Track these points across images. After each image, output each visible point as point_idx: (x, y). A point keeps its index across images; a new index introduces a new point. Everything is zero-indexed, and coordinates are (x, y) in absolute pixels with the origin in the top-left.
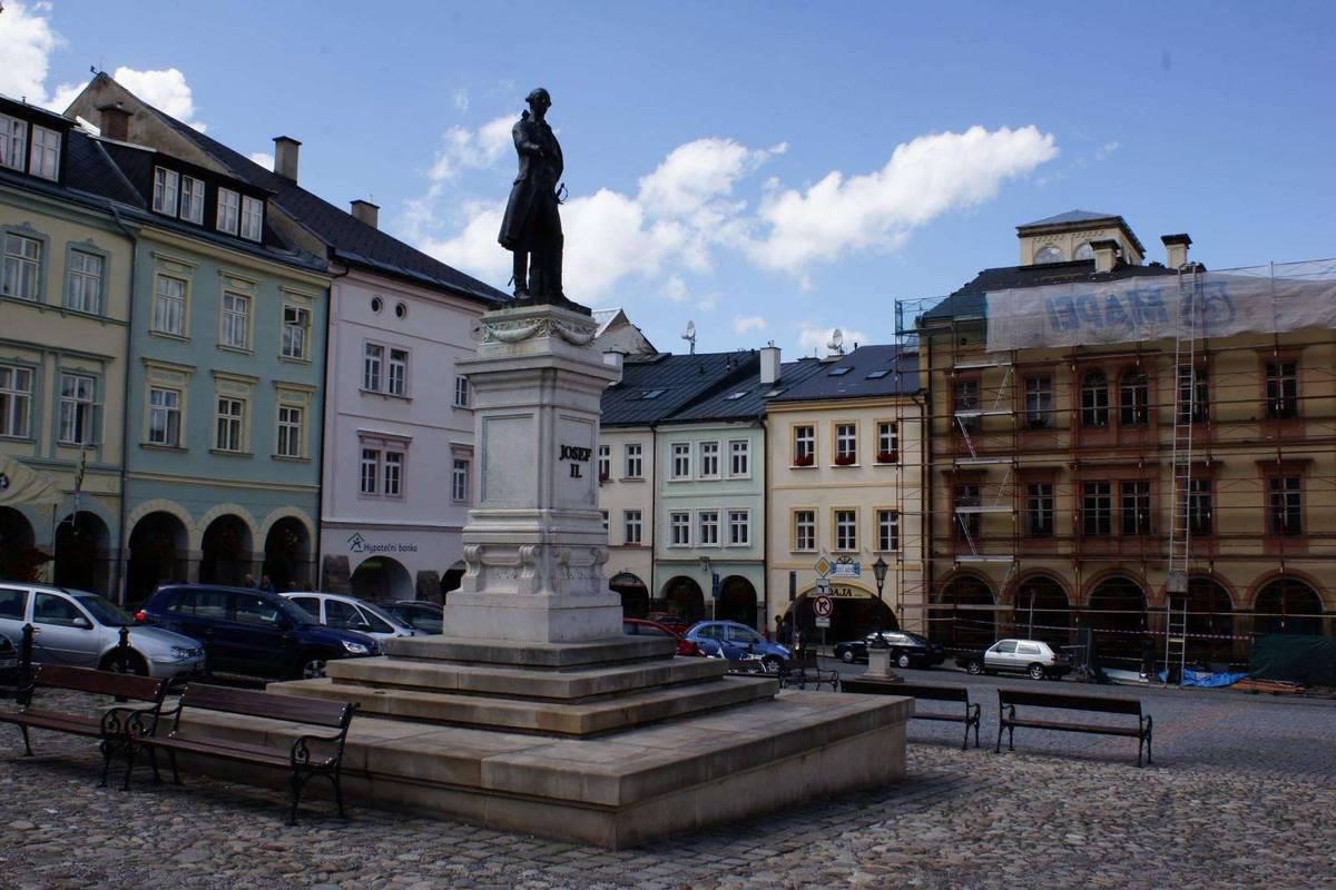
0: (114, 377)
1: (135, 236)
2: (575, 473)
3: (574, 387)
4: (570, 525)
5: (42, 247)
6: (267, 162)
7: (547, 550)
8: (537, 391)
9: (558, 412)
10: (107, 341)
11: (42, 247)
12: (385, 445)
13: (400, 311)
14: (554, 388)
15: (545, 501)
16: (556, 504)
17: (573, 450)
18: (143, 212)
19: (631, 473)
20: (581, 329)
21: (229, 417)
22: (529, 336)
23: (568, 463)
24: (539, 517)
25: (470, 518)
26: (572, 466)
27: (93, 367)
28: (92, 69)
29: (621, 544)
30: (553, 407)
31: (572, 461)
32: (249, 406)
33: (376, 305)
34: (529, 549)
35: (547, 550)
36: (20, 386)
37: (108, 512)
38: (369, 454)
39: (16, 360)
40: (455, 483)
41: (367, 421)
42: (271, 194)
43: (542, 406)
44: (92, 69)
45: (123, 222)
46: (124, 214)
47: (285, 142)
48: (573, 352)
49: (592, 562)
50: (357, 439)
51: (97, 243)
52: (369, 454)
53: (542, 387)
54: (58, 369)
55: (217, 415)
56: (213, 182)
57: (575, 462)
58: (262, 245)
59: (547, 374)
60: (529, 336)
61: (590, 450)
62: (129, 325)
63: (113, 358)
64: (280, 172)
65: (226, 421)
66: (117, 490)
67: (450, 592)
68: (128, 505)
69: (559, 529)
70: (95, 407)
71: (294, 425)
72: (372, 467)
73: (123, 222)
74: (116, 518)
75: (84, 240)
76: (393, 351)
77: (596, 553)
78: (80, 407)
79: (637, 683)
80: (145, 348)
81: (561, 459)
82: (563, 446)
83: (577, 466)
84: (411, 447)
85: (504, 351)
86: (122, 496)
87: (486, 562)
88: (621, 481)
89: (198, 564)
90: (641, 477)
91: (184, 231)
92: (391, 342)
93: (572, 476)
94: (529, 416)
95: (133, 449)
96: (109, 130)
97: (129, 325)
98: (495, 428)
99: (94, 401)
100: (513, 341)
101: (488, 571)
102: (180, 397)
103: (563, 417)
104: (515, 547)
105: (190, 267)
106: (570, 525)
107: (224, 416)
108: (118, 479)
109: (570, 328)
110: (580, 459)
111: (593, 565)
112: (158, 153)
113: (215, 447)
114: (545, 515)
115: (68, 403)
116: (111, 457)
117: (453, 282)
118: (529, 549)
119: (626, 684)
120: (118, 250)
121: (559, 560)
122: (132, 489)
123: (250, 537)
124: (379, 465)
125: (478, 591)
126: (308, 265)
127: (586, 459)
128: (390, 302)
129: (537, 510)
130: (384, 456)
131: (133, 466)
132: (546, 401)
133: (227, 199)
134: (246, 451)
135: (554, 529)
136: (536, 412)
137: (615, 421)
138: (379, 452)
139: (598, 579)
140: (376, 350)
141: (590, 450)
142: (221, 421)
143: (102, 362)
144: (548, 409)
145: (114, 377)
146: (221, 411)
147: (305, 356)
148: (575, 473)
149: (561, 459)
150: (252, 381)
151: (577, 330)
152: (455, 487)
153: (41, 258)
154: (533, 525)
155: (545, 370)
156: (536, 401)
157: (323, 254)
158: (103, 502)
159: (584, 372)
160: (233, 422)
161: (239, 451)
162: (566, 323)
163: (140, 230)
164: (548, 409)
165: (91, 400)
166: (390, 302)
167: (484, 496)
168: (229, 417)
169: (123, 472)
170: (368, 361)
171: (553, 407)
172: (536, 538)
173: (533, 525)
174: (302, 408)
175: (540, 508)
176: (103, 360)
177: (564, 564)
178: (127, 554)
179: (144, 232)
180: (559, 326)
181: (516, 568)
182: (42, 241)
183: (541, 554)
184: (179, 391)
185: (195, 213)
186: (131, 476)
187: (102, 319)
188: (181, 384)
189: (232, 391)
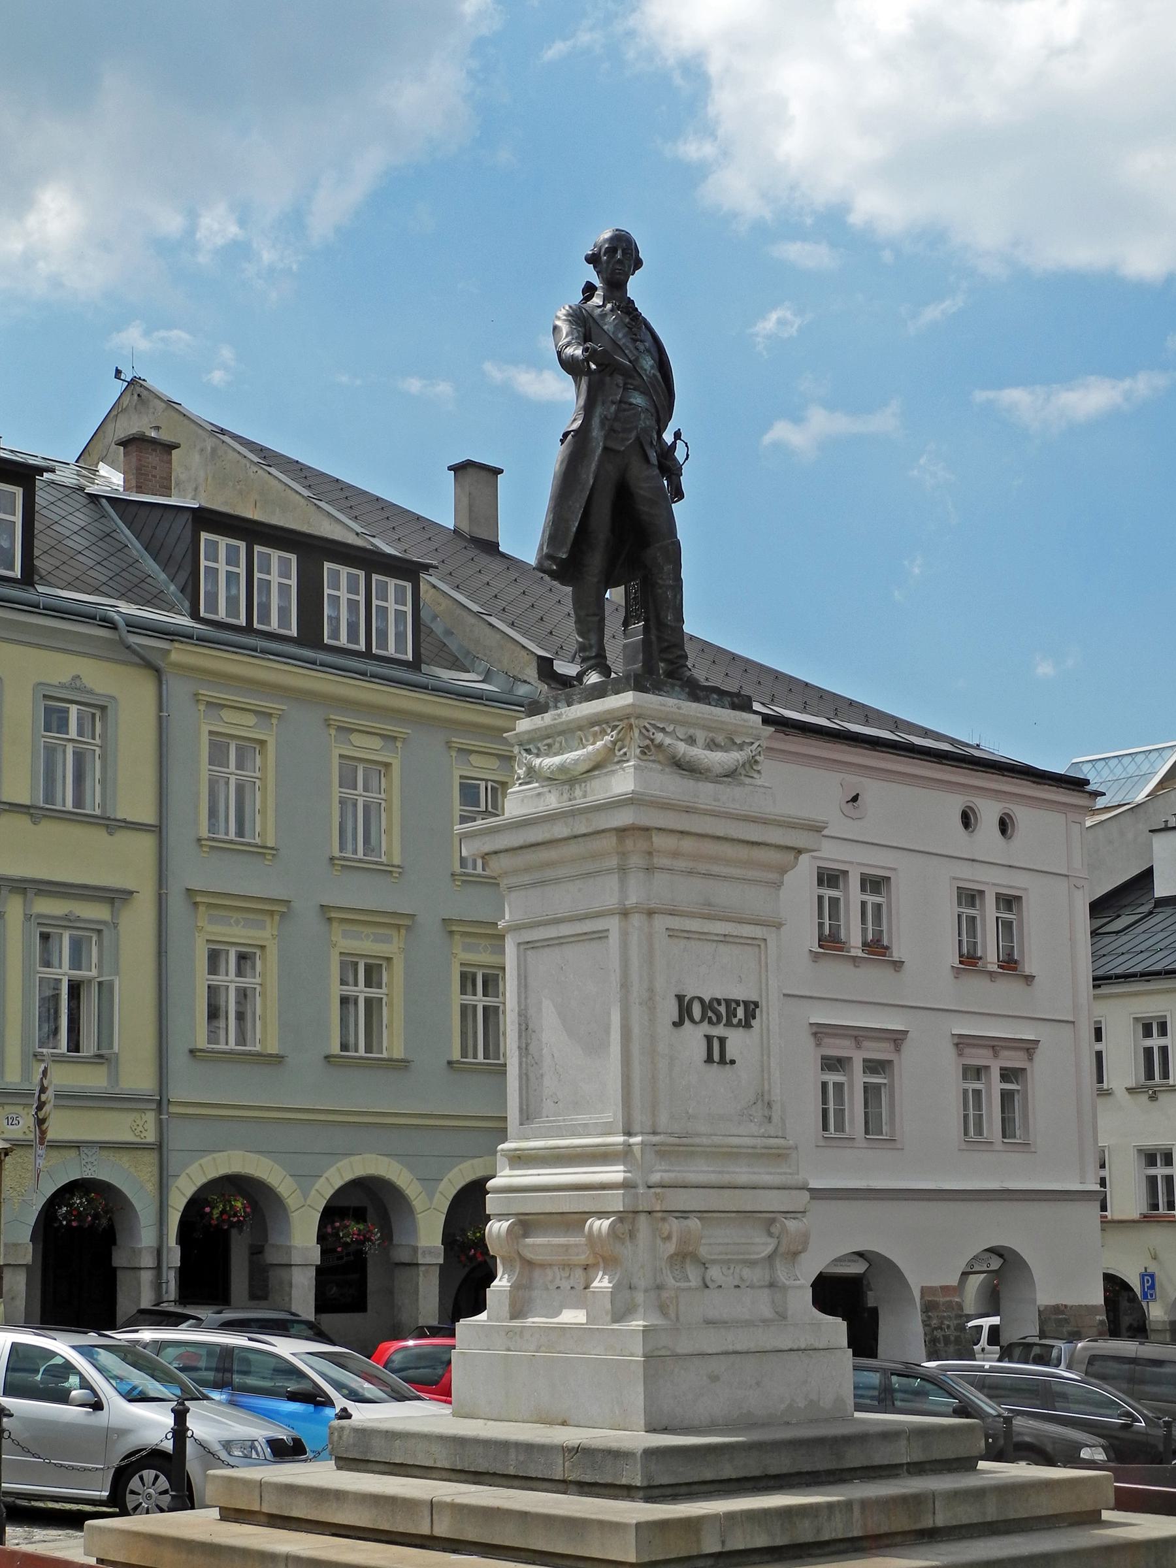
0: (137, 926)
1: (161, 664)
2: (717, 1054)
3: (702, 867)
4: (700, 1172)
5: (104, 718)
6: (441, 507)
7: (643, 1221)
8: (613, 881)
9: (661, 923)
10: (125, 862)
11: (104, 718)
12: (859, 1046)
13: (1004, 825)
14: (649, 870)
15: (640, 1118)
16: (663, 1120)
17: (709, 1007)
18: (185, 621)
19: (1150, 1075)
20: (720, 739)
21: (361, 991)
22: (597, 766)
23: (694, 1036)
24: (623, 1155)
25: (501, 1161)
26: (709, 1039)
27: (96, 912)
28: (118, 373)
29: (1135, 1215)
30: (650, 913)
31: (705, 1028)
32: (398, 965)
33: (967, 819)
34: (601, 1225)
35: (643, 1221)
36: (76, 963)
37: (132, 1179)
38: (832, 1064)
39: (66, 917)
40: (825, 1101)
41: (886, 1008)
42: (426, 567)
43: (625, 913)
44: (118, 373)
45: (133, 639)
46: (135, 626)
47: (470, 470)
48: (705, 793)
49: (770, 1249)
50: (811, 1041)
51: (89, 681)
52: (832, 1064)
53: (623, 870)
54: (28, 917)
55: (457, 999)
56: (313, 551)
57: (719, 1031)
58: (415, 665)
59: (629, 844)
60: (597, 766)
61: (756, 1005)
62: (158, 830)
63: (131, 893)
64: (465, 527)
65: (475, 1007)
66: (151, 1137)
67: (462, 1321)
68: (174, 1160)
69: (668, 1177)
70: (100, 983)
71: (373, 992)
72: (839, 1086)
73: (133, 639)
74: (151, 1187)
75: (65, 679)
76: (999, 897)
77: (775, 1230)
78: (75, 989)
79: (834, 1530)
80: (192, 871)
81: (678, 1024)
82: (680, 998)
83: (722, 1041)
84: (906, 1047)
85: (552, 801)
86: (159, 1147)
87: (529, 1255)
88: (1130, 1090)
89: (312, 1273)
90: (1171, 1081)
91: (364, 674)
92: (992, 881)
93: (709, 1059)
94: (601, 936)
95: (178, 1061)
96: (139, 478)
97: (158, 830)
98: (544, 963)
99: (100, 974)
100: (567, 779)
101: (537, 1273)
102: (264, 959)
103: (672, 933)
104: (573, 1221)
105: (395, 738)
106: (700, 1172)
107: (469, 999)
108: (150, 1117)
109: (691, 740)
110: (729, 1024)
111: (771, 1258)
112: (200, 509)
113: (456, 1055)
114: (637, 1150)
115: (218, 987)
116: (138, 1077)
117: (867, 722)
118: (601, 1225)
119: (805, 1533)
120: (132, 696)
121: (671, 1247)
122: (180, 1137)
123: (414, 1219)
124: (851, 1086)
125: (514, 1316)
126: (505, 697)
127: (747, 1025)
128: (989, 813)
129: (620, 1139)
130: (858, 1066)
131: (177, 1093)
132: (632, 900)
133: (341, 585)
134: (396, 1056)
135: (656, 1178)
136: (613, 924)
137: (1118, 971)
138: (987, 1068)
139: (784, 1289)
140: (969, 897)
141: (756, 1005)
142: (466, 1011)
143: (112, 901)
144: (636, 920)
145: (137, 926)
146: (463, 991)
147: (389, 853)
148: (717, 1054)
149: (678, 1024)
150: (277, 910)
151: (712, 745)
152: (966, 1117)
153: (103, 736)
154: (614, 1173)
155: (622, 832)
156: (611, 900)
157: (531, 673)
158: (125, 1160)
159: (720, 833)
160: (369, 1002)
161: (385, 1055)
162: (681, 732)
163: (169, 651)
164: (636, 920)
165: (94, 973)
166: (989, 813)
167: (526, 1116)
168: (479, 1000)
169: (161, 1104)
170: (820, 898)
171: (650, 913)
172: (616, 1201)
173: (614, 1173)
174: (389, 959)
175: (628, 1133)
176: (116, 897)
177: (684, 1257)
178: (174, 1256)
179: (174, 657)
180: (659, 737)
181: (586, 1268)
182: (103, 709)
183: (632, 1234)
184: (263, 947)
185: (281, 615)
186: (173, 1109)
187: (111, 824)
188: (265, 934)
189: (367, 945)
